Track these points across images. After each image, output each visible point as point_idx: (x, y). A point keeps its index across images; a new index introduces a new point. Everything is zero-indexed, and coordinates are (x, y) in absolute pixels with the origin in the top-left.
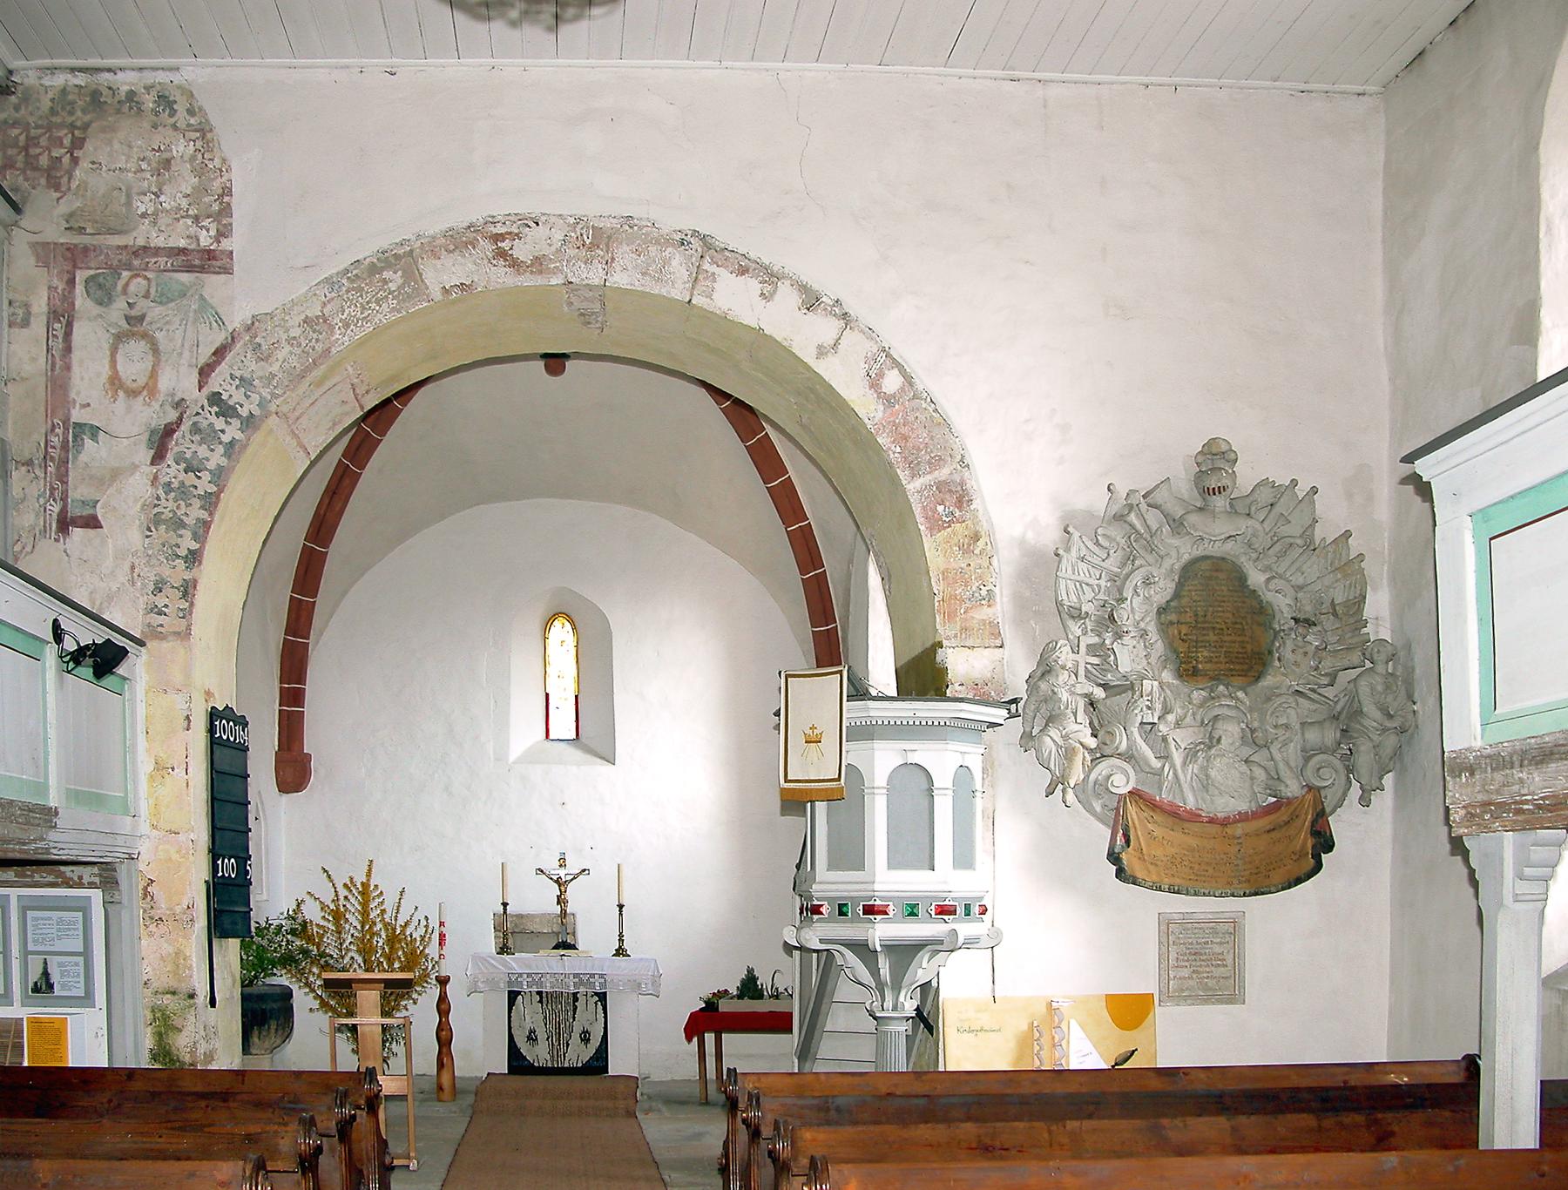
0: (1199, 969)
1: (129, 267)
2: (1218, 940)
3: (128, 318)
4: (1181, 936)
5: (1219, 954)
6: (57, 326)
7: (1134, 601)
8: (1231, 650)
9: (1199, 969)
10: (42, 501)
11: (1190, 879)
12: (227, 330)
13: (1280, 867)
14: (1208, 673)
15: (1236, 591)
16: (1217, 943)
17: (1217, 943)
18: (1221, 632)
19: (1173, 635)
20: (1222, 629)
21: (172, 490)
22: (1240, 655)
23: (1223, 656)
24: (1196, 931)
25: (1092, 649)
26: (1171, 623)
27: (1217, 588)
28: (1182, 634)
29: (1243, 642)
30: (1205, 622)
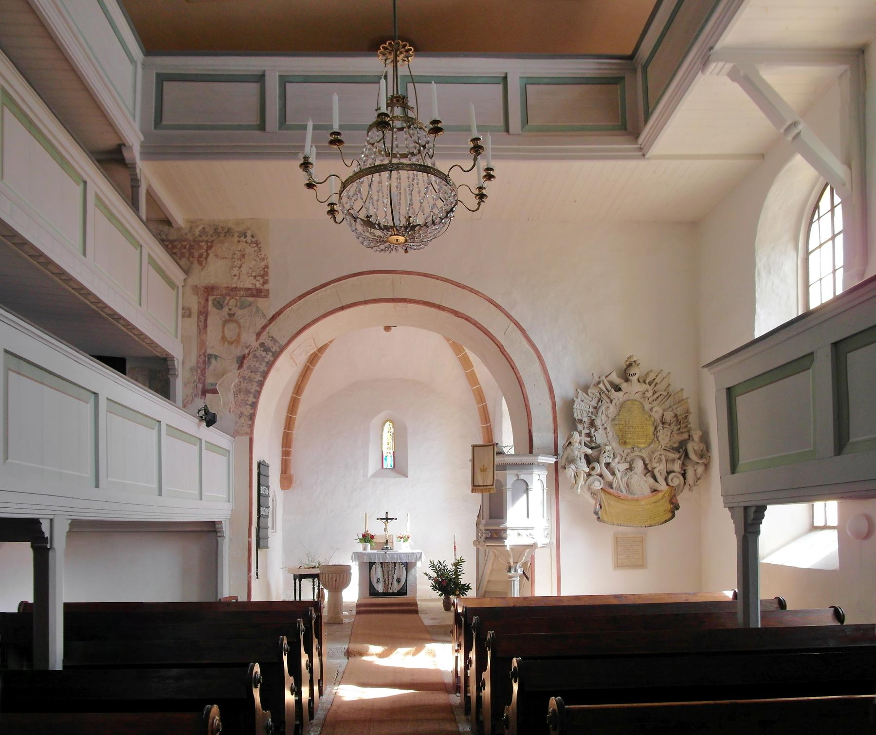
1: (229, 295)
3: (229, 315)
6: (201, 317)
10: (195, 383)
12: (266, 319)
21: (245, 380)
26: (616, 425)
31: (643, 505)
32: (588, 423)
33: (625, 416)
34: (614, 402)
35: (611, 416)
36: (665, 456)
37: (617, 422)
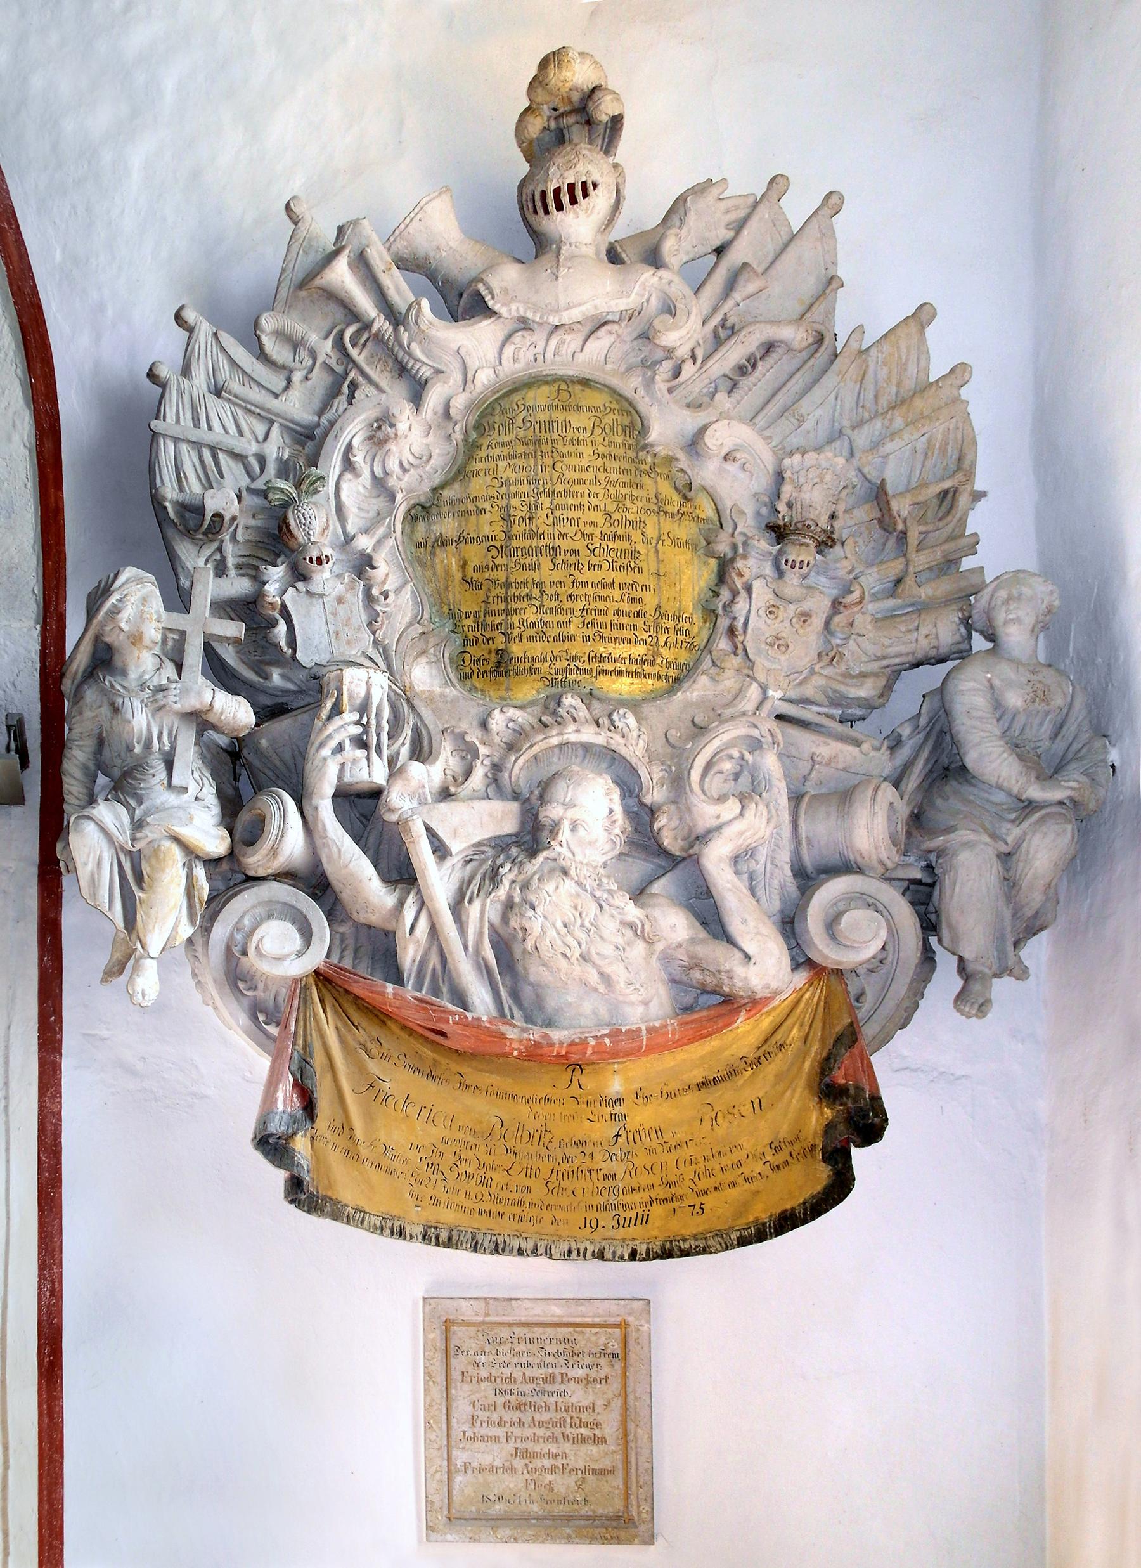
0: (530, 1446)
2: (580, 1373)
4: (483, 1358)
5: (582, 1409)
7: (344, 486)
8: (601, 605)
9: (530, 1446)
11: (480, 1212)
13: (733, 1184)
14: (538, 665)
15: (616, 458)
16: (578, 1381)
17: (578, 1381)
18: (572, 559)
19: (447, 571)
20: (577, 553)
22: (625, 620)
24: (522, 1347)
25: (227, 608)
26: (442, 542)
27: (564, 450)
28: (470, 569)
29: (634, 585)
31: (618, 1101)
34: (434, 398)
37: (448, 527)
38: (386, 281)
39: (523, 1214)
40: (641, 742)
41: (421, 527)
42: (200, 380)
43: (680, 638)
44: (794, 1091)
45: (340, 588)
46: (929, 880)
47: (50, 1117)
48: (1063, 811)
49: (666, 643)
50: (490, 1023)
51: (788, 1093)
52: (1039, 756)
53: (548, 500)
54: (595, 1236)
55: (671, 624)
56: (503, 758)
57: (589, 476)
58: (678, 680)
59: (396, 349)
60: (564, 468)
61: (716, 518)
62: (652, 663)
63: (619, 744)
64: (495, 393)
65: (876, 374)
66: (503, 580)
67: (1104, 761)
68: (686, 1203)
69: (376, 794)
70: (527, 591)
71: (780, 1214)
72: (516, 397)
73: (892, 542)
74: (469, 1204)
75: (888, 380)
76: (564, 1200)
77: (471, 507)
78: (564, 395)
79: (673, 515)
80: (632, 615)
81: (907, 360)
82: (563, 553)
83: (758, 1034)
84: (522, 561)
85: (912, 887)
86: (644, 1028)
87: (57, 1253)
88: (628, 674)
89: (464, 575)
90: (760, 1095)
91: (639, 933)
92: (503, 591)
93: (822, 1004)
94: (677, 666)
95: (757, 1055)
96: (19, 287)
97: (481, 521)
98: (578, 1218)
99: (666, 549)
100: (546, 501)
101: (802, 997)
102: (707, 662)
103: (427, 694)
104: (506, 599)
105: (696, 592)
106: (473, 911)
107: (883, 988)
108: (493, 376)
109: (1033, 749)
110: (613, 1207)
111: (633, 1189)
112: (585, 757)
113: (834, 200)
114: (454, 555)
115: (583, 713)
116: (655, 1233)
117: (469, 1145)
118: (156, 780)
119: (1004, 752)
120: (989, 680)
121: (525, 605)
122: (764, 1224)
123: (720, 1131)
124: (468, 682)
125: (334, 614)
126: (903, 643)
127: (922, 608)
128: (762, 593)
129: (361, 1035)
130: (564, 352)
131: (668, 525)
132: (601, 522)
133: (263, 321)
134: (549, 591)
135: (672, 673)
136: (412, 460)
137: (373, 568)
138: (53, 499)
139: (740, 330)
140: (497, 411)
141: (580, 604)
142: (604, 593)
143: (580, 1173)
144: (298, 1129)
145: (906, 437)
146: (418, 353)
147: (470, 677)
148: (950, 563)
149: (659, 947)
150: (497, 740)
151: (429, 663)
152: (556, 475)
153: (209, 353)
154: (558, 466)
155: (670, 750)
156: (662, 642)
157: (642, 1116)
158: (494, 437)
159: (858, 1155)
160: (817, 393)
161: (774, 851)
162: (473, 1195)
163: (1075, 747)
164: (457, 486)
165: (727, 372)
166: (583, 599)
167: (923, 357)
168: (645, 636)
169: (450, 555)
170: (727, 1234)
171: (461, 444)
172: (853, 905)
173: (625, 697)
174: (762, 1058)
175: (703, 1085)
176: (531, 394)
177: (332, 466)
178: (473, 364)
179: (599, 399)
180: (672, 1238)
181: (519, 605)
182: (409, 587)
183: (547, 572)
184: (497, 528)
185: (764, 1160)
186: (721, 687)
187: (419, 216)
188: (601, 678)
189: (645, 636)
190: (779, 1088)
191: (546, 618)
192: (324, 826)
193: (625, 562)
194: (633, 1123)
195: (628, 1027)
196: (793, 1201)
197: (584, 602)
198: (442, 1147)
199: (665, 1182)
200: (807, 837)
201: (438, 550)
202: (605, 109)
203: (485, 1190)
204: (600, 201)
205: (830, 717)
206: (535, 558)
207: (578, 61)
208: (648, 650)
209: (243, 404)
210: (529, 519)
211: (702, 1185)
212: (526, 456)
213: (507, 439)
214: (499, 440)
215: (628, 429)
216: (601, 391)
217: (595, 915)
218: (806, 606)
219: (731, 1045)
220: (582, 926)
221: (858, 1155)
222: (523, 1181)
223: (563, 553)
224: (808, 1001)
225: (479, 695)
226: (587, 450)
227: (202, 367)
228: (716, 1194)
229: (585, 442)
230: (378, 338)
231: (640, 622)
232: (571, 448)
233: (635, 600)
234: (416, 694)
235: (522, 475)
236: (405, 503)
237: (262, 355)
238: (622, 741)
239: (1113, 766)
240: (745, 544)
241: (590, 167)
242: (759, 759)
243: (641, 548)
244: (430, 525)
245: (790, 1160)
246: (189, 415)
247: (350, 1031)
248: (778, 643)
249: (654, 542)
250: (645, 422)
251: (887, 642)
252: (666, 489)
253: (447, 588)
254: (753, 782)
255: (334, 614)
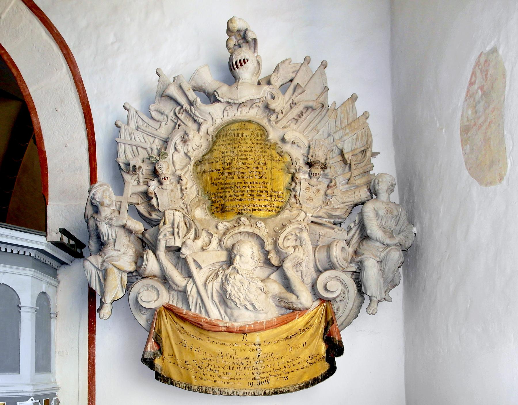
8: (253, 189)
11: (215, 381)
13: (298, 370)
14: (234, 208)
18: (244, 175)
19: (207, 181)
20: (245, 173)
22: (261, 194)
23: (246, 194)
26: (205, 172)
29: (264, 182)
30: (231, 168)
31: (259, 344)
32: (148, 172)
33: (224, 153)
34: (203, 129)
35: (196, 155)
36: (310, 234)
37: (206, 167)
38: (188, 93)
39: (229, 382)
40: (266, 231)
41: (199, 167)
42: (133, 126)
43: (280, 199)
44: (316, 340)
45: (172, 187)
46: (359, 271)
47: (92, 354)
48: (397, 248)
49: (275, 200)
50: (215, 321)
51: (315, 340)
52: (392, 231)
53: (237, 157)
54: (252, 388)
55: (276, 194)
56: (222, 237)
57: (250, 149)
58: (279, 212)
59: (191, 114)
60: (241, 147)
61: (291, 161)
62: (270, 207)
63: (257, 232)
64: (222, 126)
65: (340, 116)
66: (223, 183)
67: (412, 232)
68: (281, 376)
69: (179, 249)
70: (230, 186)
71: (313, 379)
72: (228, 127)
73: (347, 167)
74: (211, 379)
75: (344, 117)
76: (242, 377)
77: (213, 161)
78: (243, 126)
79: (276, 161)
80: (263, 192)
81: (349, 112)
82: (241, 173)
83: (304, 322)
84: (229, 176)
85: (354, 274)
86: (265, 321)
87: (94, 396)
88: (263, 210)
89: (211, 182)
90: (306, 341)
91: (262, 291)
92: (223, 186)
93: (325, 312)
94: (279, 207)
95: (304, 328)
96: (83, 102)
97: (216, 165)
98: (246, 382)
99: (274, 171)
100: (236, 158)
101: (318, 309)
102: (288, 206)
103: (200, 219)
104: (224, 188)
105: (284, 184)
106: (210, 286)
107: (345, 306)
108: (221, 121)
109: (389, 229)
110: (258, 378)
111: (264, 373)
112: (249, 237)
113: (324, 63)
114: (208, 175)
115: (247, 222)
116: (271, 386)
117: (211, 360)
118: (110, 248)
119: (378, 230)
120: (374, 207)
121: (229, 190)
122: (308, 382)
123: (292, 353)
124: (213, 215)
125: (170, 195)
126: (350, 198)
127: (357, 187)
128: (304, 184)
129: (178, 326)
130: (243, 113)
131: (274, 164)
132: (253, 163)
133: (151, 107)
134: (237, 185)
135: (277, 209)
136: (196, 147)
137: (182, 180)
138: (93, 165)
139: (297, 104)
140: (222, 131)
141: (247, 189)
142: (255, 185)
143: (246, 368)
144: (156, 357)
145: (350, 135)
146: (197, 114)
147: (214, 213)
148: (366, 172)
149: (270, 295)
150: (221, 232)
151: (201, 209)
152: (239, 150)
153: (135, 117)
154: (240, 147)
155: (274, 233)
156: (273, 199)
157: (266, 349)
158: (221, 139)
159: (337, 359)
160: (323, 122)
161: (307, 264)
162: (212, 376)
163: (403, 228)
164: (209, 154)
165: (294, 117)
166: (248, 187)
167: (354, 110)
168: (268, 198)
169: (207, 176)
170: (295, 386)
171: (211, 142)
172: (333, 280)
173: (262, 217)
174: (306, 329)
175: (286, 338)
176: (233, 126)
177: (171, 150)
178: (215, 117)
179: (253, 126)
180: (277, 388)
181: (228, 190)
182: (195, 186)
183: (236, 179)
184: (221, 166)
185: (307, 362)
186: (292, 213)
187: (197, 73)
188: (254, 212)
189: (268, 198)
190: (312, 339)
191: (236, 194)
192: (162, 261)
193: (261, 175)
194: (263, 352)
195: (260, 321)
196: (318, 375)
197: (248, 188)
198: (203, 361)
199: (275, 370)
200: (318, 259)
201: (204, 175)
202: (250, 36)
203: (217, 374)
204: (250, 65)
205: (329, 222)
206: (232, 175)
207: (238, 21)
208: (269, 202)
209: (145, 132)
210: (231, 163)
211: (287, 370)
212: (230, 144)
213: (225, 139)
214: (222, 140)
215: (262, 135)
216: (254, 124)
217: (248, 286)
218: (318, 187)
219: (296, 326)
220: (243, 289)
221: (337, 359)
222: (228, 371)
223: (241, 173)
224: (320, 311)
225: (217, 218)
226: (249, 142)
227: (133, 122)
228: (292, 373)
229: (248, 139)
230: (186, 110)
231: (266, 194)
232: (243, 141)
233: (264, 187)
234: (196, 218)
235: (229, 150)
236: (193, 161)
237: (152, 118)
238: (258, 231)
239: (415, 233)
240: (299, 169)
241: (245, 54)
242: (301, 235)
243: (266, 171)
244: (201, 167)
245: (316, 361)
246: (128, 136)
247: (174, 325)
248: (310, 199)
249: (270, 169)
250: (268, 133)
251: (345, 198)
252: (274, 153)
253: (206, 186)
254: (301, 242)
255: (170, 195)
